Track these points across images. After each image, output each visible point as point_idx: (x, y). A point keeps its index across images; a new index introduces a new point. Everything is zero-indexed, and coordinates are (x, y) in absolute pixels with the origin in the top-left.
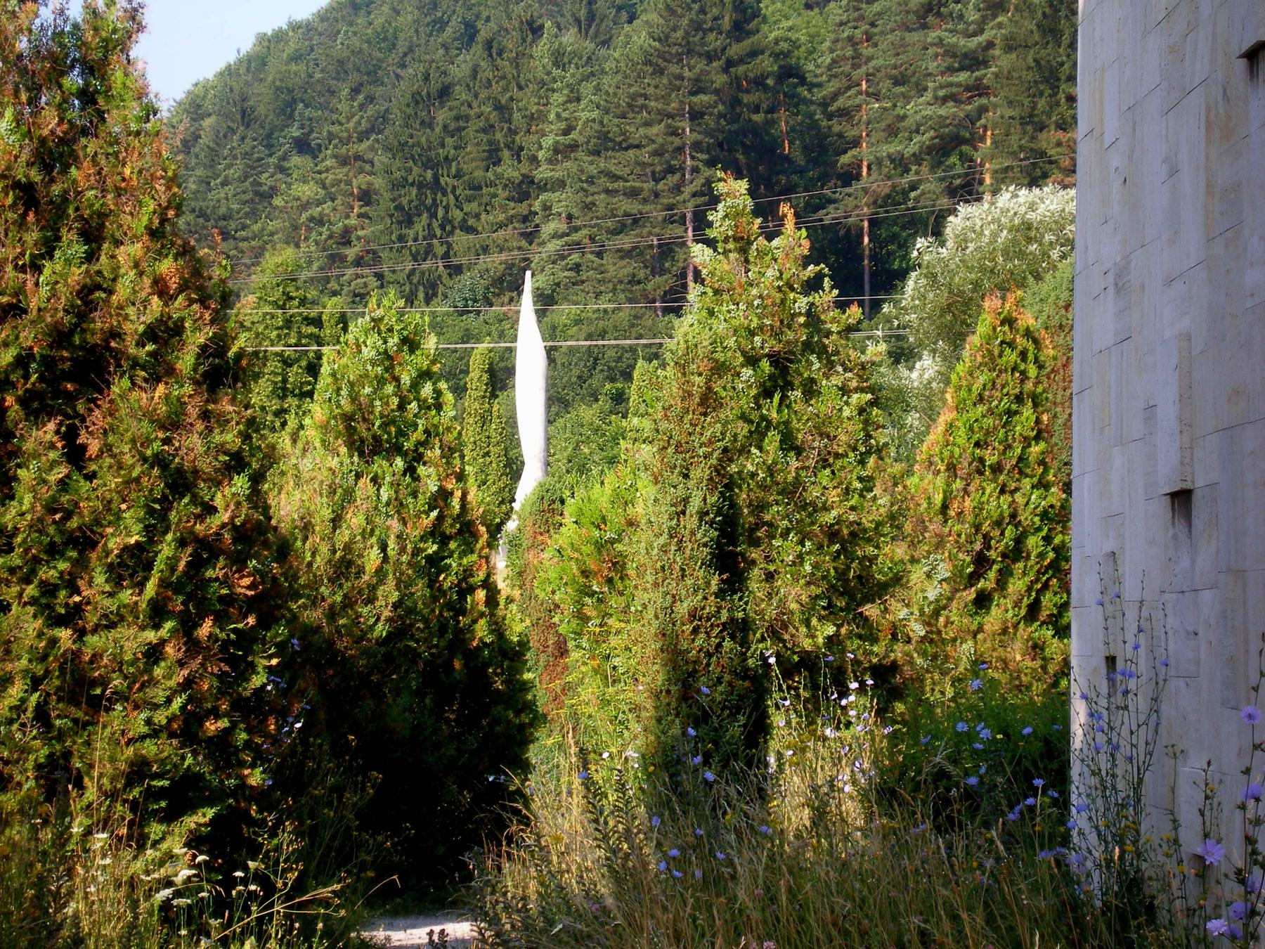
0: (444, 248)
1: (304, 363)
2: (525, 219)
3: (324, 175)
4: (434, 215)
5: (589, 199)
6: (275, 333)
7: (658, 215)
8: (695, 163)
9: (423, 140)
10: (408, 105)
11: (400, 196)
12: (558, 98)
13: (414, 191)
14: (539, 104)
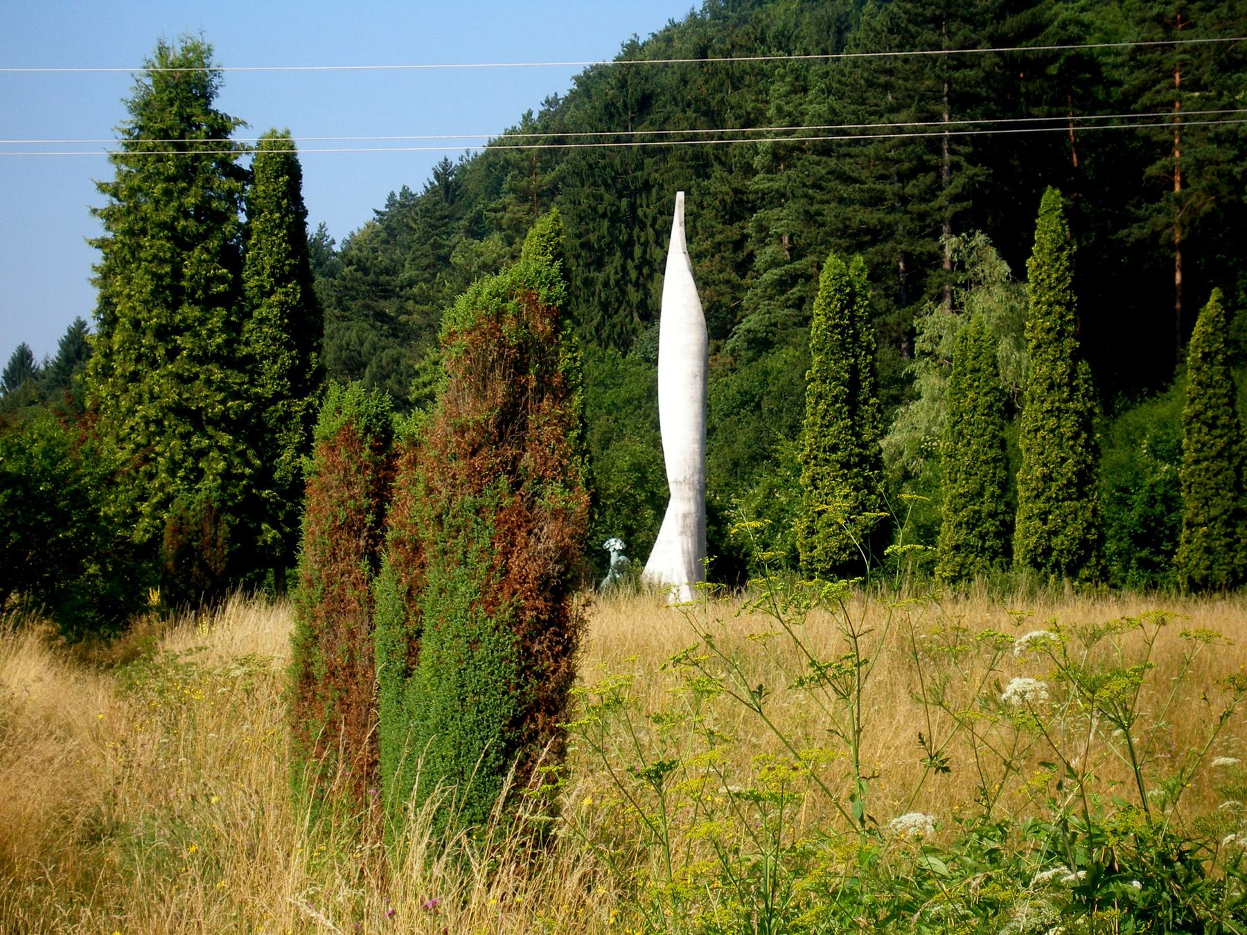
0: (640, 295)
1: (213, 244)
2: (738, 245)
3: (499, 215)
4: (628, 255)
5: (816, 207)
6: (161, 186)
7: (902, 222)
8: (956, 158)
9: (617, 161)
10: (600, 120)
11: (587, 231)
12: (778, 88)
13: (606, 223)
14: (757, 100)
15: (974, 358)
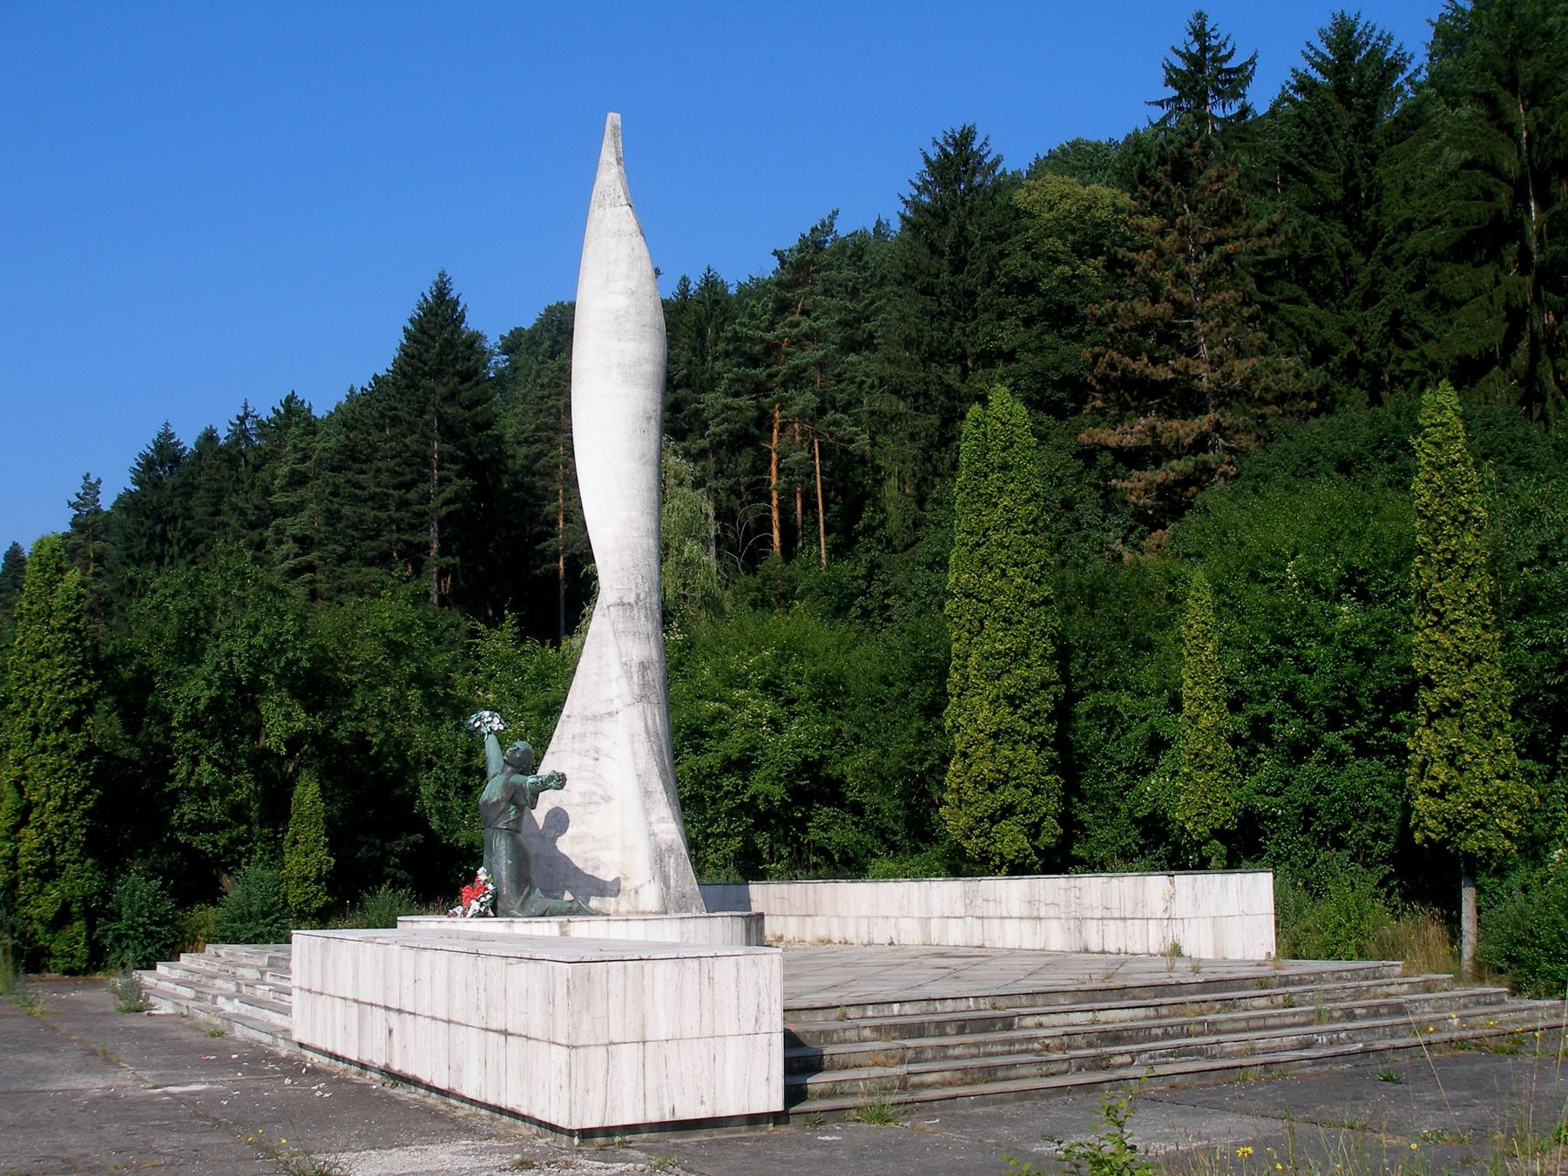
15: (1004, 449)
